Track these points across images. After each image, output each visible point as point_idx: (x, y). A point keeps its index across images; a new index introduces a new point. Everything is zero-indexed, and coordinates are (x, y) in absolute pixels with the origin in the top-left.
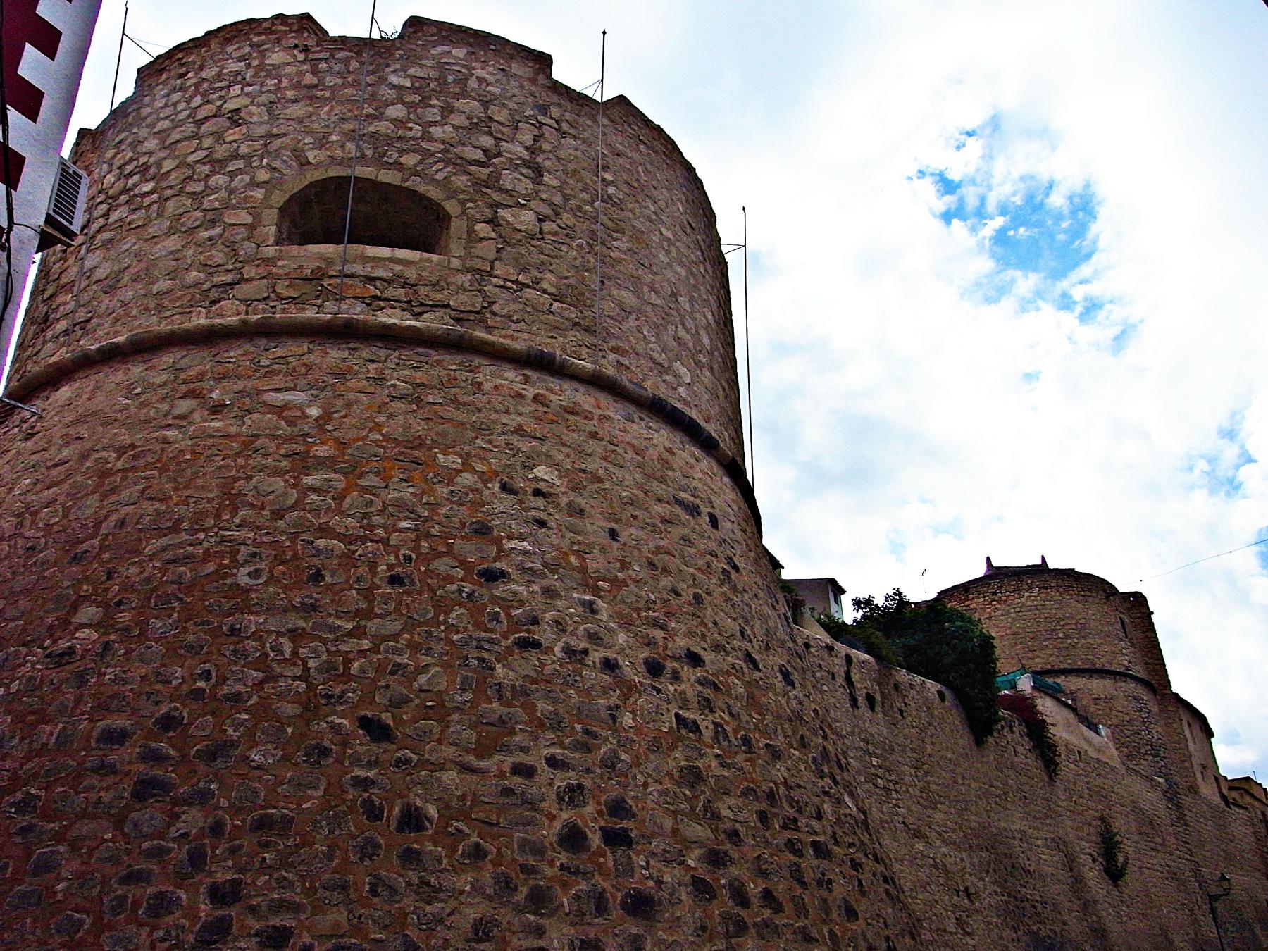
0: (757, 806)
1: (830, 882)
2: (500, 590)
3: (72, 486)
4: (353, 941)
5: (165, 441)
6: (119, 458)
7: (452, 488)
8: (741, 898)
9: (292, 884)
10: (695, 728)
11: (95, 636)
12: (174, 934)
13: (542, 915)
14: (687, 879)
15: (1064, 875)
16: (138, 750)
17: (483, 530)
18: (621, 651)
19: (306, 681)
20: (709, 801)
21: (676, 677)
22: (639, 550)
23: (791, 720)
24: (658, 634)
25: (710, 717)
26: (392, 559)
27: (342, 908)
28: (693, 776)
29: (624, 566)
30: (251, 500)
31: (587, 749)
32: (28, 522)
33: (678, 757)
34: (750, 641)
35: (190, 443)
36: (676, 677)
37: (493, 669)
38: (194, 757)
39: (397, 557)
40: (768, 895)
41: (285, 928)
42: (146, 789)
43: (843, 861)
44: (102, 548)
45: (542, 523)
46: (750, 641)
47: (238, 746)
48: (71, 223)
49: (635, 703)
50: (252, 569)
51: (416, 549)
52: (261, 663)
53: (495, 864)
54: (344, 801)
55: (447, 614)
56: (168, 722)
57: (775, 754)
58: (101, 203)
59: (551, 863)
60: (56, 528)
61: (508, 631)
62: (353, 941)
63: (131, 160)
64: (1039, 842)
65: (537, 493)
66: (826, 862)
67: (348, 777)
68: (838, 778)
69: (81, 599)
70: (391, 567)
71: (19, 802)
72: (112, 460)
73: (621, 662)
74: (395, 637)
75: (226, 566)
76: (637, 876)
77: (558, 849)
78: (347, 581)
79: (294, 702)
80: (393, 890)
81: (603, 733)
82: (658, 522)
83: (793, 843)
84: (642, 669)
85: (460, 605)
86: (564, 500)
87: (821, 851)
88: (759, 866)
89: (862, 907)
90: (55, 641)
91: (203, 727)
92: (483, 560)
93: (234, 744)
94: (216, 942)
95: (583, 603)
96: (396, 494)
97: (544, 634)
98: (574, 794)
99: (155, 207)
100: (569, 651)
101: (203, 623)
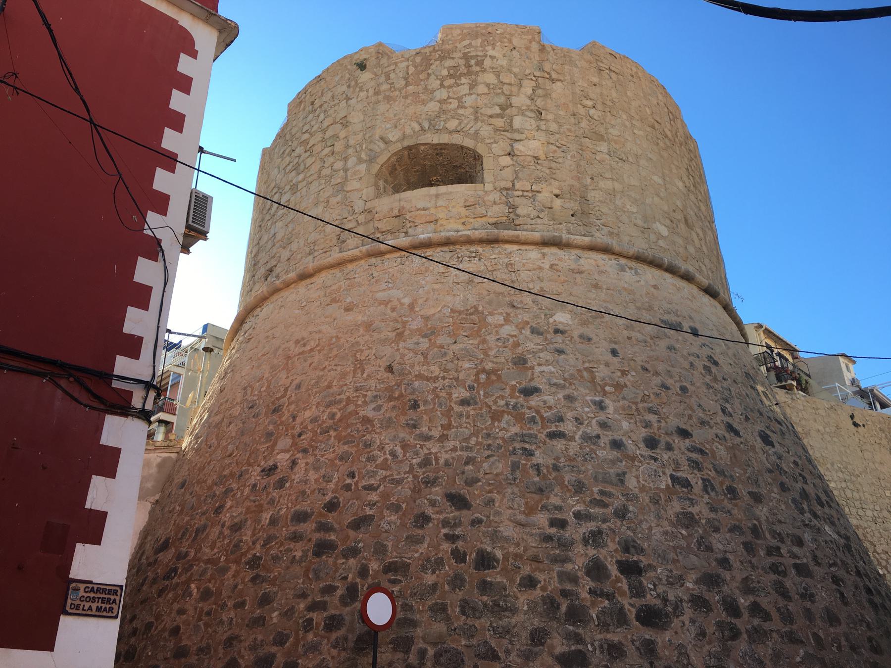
0: (743, 539)
1: (812, 595)
2: (534, 401)
8: (733, 609)
10: (686, 484)
13: (578, 627)
18: (626, 434)
21: (669, 447)
22: (635, 361)
23: (770, 471)
24: (652, 418)
32: (249, 392)
33: (676, 506)
34: (731, 415)
36: (669, 447)
40: (755, 608)
42: (322, 548)
43: (824, 578)
46: (731, 415)
48: (204, 227)
51: (477, 380)
57: (757, 498)
58: (275, 193)
63: (290, 162)
65: (557, 331)
68: (819, 513)
72: (292, 348)
73: (625, 442)
82: (649, 340)
83: (777, 566)
84: (642, 445)
85: (508, 414)
86: (576, 334)
87: (802, 570)
90: (266, 462)
93: (371, 517)
97: (568, 427)
98: (595, 538)
99: (305, 189)
100: (586, 438)
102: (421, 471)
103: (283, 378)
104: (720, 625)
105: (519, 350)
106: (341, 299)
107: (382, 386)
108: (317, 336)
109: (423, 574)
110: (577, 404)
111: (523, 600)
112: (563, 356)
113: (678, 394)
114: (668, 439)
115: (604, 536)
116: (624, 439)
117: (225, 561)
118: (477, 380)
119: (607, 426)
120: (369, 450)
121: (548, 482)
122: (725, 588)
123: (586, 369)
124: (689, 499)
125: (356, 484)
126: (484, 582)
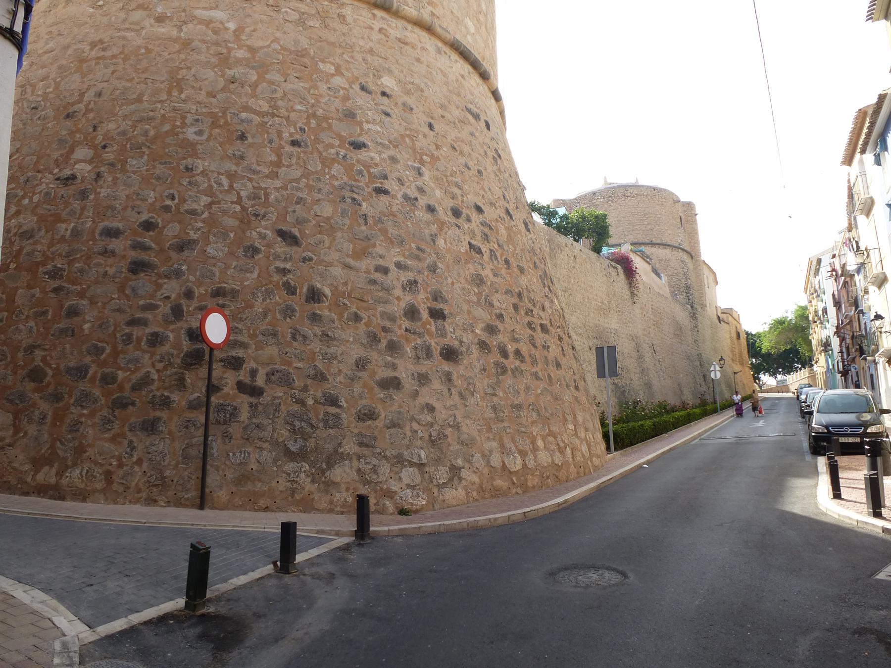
2: (363, 155)
3: (60, 67)
4: (283, 367)
5: (124, 38)
6: (92, 49)
7: (330, 86)
8: (504, 354)
9: (241, 331)
10: (479, 252)
11: (89, 168)
12: (166, 358)
14: (476, 341)
15: (634, 354)
16: (129, 242)
17: (350, 115)
19: (240, 205)
20: (488, 296)
23: (529, 252)
25: (487, 246)
26: (292, 130)
27: (274, 347)
28: (479, 281)
29: (438, 147)
30: (193, 84)
31: (418, 258)
32: (29, 90)
33: (471, 269)
34: (508, 203)
35: (144, 41)
36: (469, 220)
37: (360, 205)
38: (168, 248)
39: (295, 129)
40: (518, 353)
41: (239, 358)
44: (88, 110)
45: (387, 114)
46: (508, 203)
47: (198, 243)
49: (446, 233)
50: (197, 129)
51: (308, 124)
52: (209, 192)
53: (367, 325)
54: (271, 282)
55: (330, 169)
56: (148, 226)
59: (400, 327)
60: (51, 96)
61: (369, 182)
62: (283, 367)
64: (623, 336)
65: (384, 94)
66: (547, 335)
67: (273, 267)
69: (76, 143)
70: (291, 134)
71: (51, 272)
73: (437, 208)
74: (297, 180)
75: (178, 127)
76: (449, 337)
77: (404, 319)
78: (263, 142)
79: (233, 218)
80: (305, 337)
81: (428, 250)
82: (457, 121)
84: (450, 213)
88: (514, 336)
89: (563, 362)
90: (61, 170)
91: (172, 230)
92: (351, 135)
93: (195, 242)
94: (195, 364)
95: (414, 168)
96: (291, 86)
97: (391, 185)
98: (412, 286)
100: (406, 197)
101: (165, 163)
102: (250, 203)
103: (75, 82)
104: (497, 364)
105: (349, 104)
106: (151, 6)
107: (204, 110)
108: (122, 42)
109: (254, 301)
110: (399, 166)
111: (348, 335)
112: (388, 119)
113: (476, 176)
114: (468, 212)
115: (419, 285)
116: (436, 205)
117: (15, 269)
118: (308, 124)
119: (424, 191)
120: (191, 174)
121: (374, 232)
122: (500, 336)
123: (408, 136)
124: (481, 264)
125: (177, 206)
126: (314, 314)
